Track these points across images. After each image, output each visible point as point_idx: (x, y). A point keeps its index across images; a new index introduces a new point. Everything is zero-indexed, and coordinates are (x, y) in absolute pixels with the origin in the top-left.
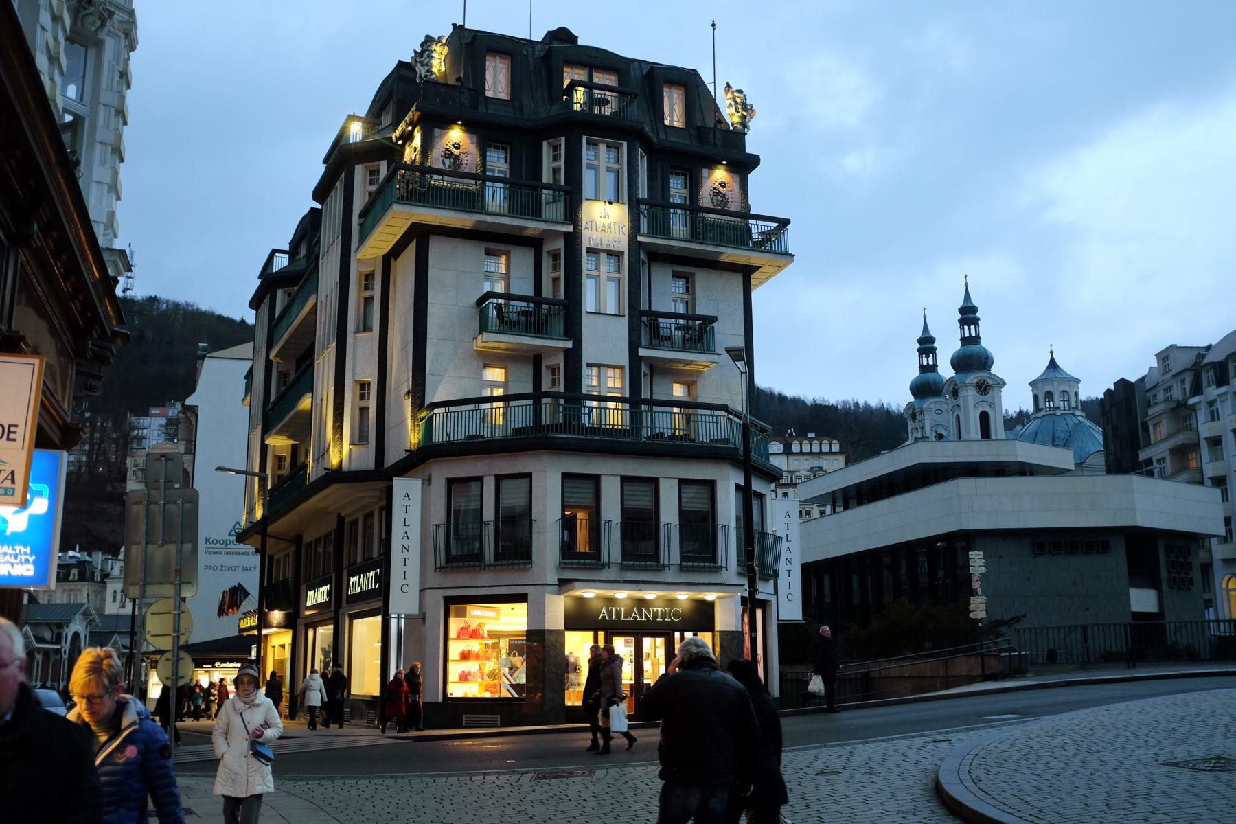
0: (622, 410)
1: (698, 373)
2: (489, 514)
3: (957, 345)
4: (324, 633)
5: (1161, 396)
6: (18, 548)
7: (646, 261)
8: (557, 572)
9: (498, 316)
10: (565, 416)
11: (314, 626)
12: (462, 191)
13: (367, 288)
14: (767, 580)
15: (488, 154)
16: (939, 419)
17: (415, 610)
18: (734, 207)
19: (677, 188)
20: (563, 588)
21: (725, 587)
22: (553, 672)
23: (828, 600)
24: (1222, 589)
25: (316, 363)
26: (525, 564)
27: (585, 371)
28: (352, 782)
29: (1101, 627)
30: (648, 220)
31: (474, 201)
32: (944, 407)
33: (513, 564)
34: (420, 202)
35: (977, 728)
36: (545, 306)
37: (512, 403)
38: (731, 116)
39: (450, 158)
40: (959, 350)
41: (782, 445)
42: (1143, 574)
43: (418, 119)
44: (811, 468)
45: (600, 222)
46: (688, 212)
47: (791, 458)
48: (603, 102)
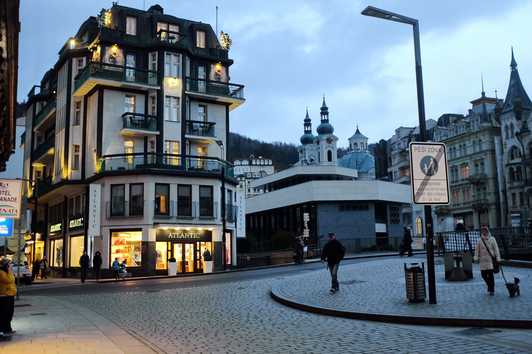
0: (178, 159)
1: (208, 144)
2: (127, 198)
3: (319, 123)
4: (58, 243)
5: (396, 147)
6: (3, 226)
7: (189, 100)
8: (153, 220)
9: (131, 121)
10: (156, 161)
11: (54, 240)
12: (117, 72)
13: (78, 107)
14: (233, 222)
15: (127, 57)
16: (312, 153)
17: (98, 234)
18: (223, 80)
19: (201, 71)
20: (155, 226)
21: (216, 226)
23: (262, 227)
24: (415, 223)
25: (56, 136)
26: (141, 217)
27: (164, 143)
28: (84, 295)
29: (364, 239)
30: (190, 84)
31: (122, 76)
32: (314, 148)
33: (136, 217)
34: (100, 76)
35: (294, 275)
36: (149, 118)
37: (136, 156)
38: (223, 44)
40: (320, 125)
41: (248, 162)
42: (381, 217)
43: (99, 42)
44: (260, 171)
45: (171, 86)
46: (205, 82)
47: (252, 167)
48: (173, 38)
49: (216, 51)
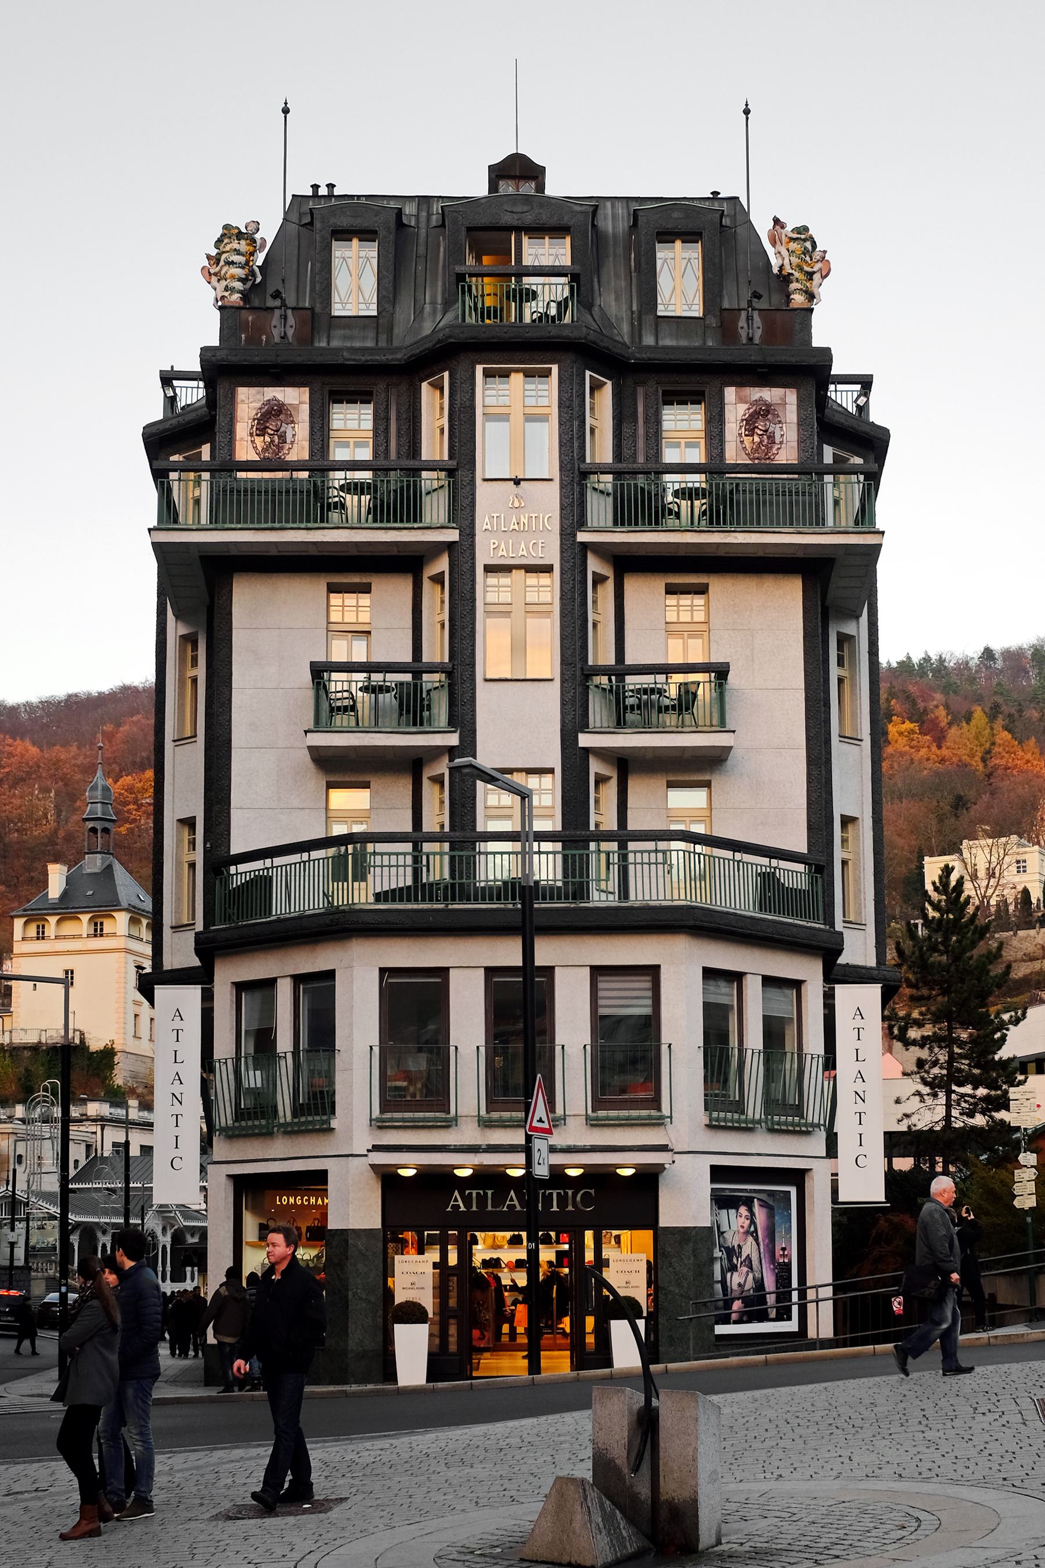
22: (361, 1299)
39: (263, 435)
49: (749, 318)
